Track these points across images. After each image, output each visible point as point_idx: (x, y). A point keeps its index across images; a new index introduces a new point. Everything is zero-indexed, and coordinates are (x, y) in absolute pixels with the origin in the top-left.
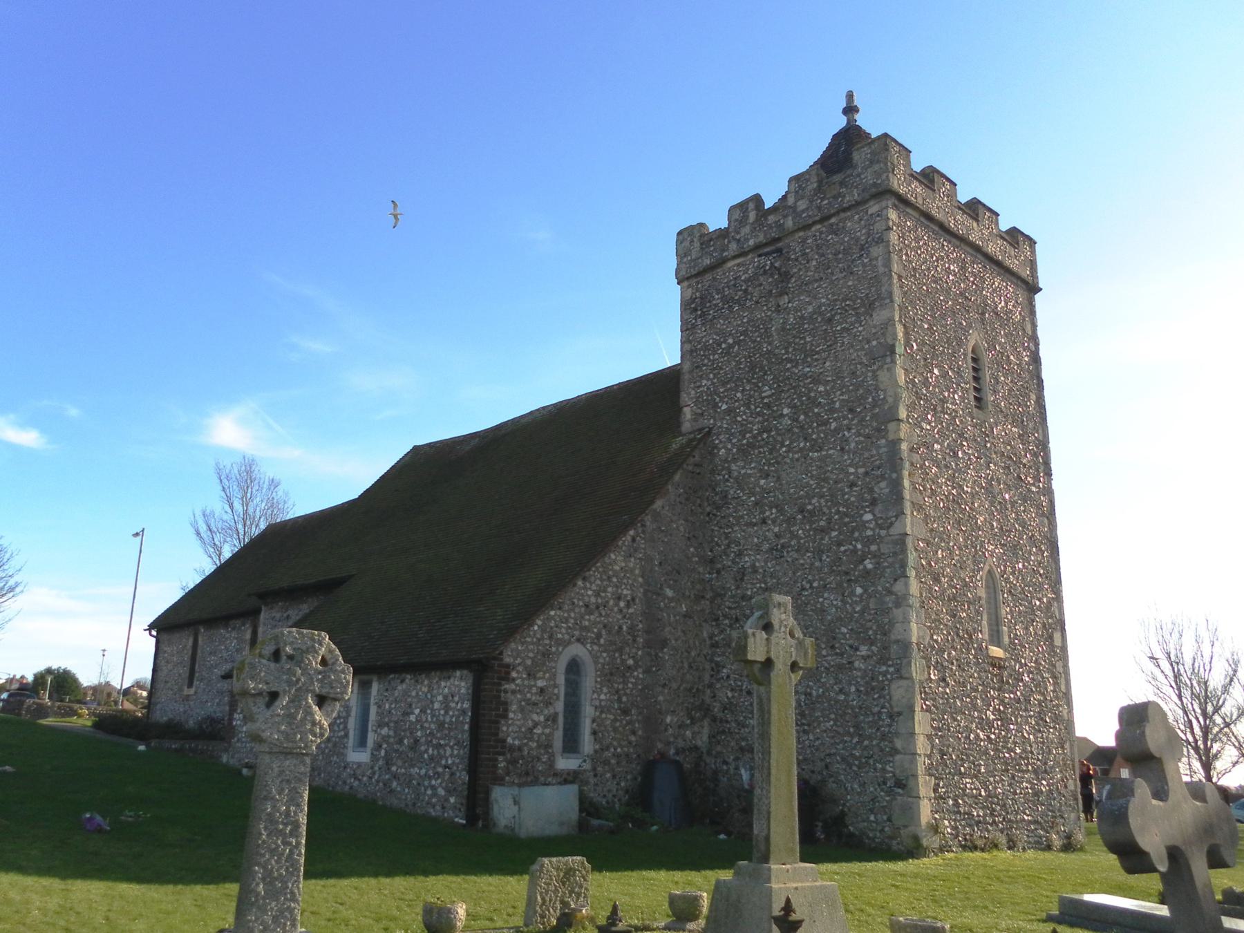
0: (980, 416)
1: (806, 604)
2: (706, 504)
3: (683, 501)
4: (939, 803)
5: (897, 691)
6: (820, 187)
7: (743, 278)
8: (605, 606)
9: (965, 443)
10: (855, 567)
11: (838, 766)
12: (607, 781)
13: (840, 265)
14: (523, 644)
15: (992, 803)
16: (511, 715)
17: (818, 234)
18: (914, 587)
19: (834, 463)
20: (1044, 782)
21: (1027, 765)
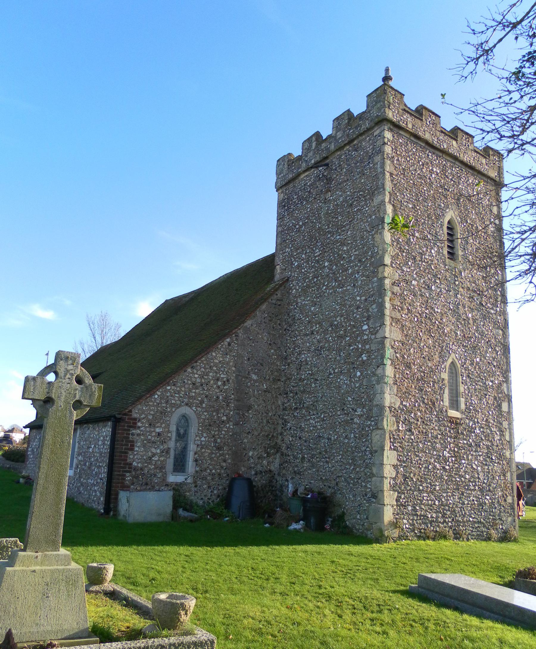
0: (451, 264)
1: (331, 383)
2: (284, 323)
3: (267, 321)
4: (400, 508)
5: (375, 437)
6: (349, 122)
7: (308, 184)
8: (207, 384)
9: (438, 281)
10: (357, 359)
11: (343, 484)
12: (204, 490)
13: (358, 170)
14: (147, 406)
15: (444, 509)
16: (136, 449)
17: (347, 152)
18: (389, 371)
19: (349, 294)
20: (488, 497)
21: (474, 486)
